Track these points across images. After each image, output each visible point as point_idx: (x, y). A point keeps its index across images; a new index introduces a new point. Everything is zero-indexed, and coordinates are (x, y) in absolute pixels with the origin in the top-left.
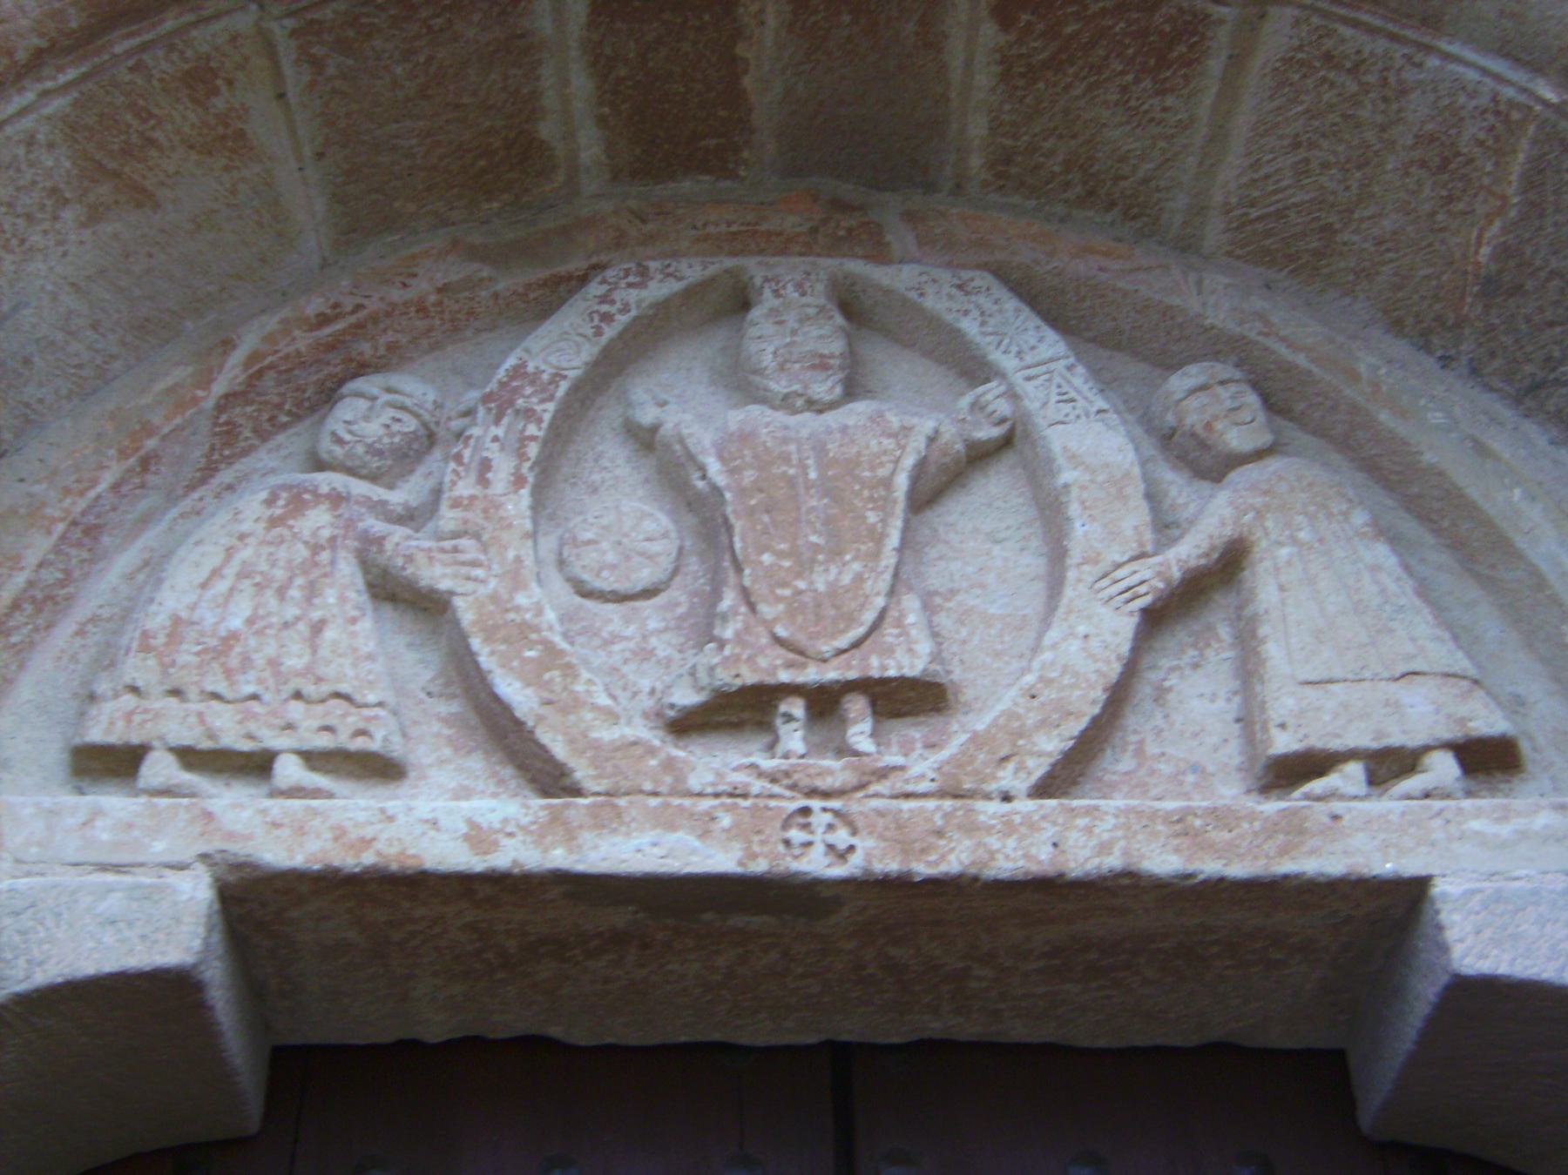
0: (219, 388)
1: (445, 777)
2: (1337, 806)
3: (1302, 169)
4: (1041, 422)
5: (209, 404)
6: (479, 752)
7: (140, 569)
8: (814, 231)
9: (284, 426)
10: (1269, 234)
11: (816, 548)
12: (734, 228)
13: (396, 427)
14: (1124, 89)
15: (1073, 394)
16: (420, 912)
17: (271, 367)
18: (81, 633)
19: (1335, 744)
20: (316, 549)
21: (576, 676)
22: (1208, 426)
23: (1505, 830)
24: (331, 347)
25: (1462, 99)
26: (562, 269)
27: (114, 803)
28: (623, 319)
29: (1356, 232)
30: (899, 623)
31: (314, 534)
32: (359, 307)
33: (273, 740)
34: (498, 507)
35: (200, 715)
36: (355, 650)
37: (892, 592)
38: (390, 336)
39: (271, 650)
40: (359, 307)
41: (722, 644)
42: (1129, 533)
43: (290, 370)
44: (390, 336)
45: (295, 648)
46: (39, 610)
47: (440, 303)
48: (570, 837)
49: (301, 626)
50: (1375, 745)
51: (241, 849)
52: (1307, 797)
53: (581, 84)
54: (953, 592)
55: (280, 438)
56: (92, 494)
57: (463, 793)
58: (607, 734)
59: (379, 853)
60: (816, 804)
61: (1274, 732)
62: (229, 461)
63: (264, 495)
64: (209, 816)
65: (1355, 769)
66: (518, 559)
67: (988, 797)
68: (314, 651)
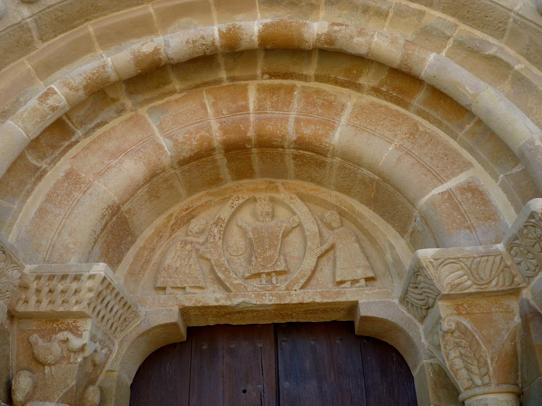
0: (171, 223)
1: (211, 289)
2: (346, 290)
3: (344, 181)
4: (303, 224)
5: (170, 226)
6: (242, 48)
7: (161, 254)
8: (267, 188)
9: (182, 227)
10: (341, 188)
11: (267, 249)
12: (253, 188)
13: (200, 228)
14: (315, 169)
15: (309, 218)
16: (209, 310)
17: (179, 218)
18: (153, 266)
19: (346, 279)
20: (189, 252)
21: (230, 273)
22: (330, 223)
23: (370, 292)
24: (189, 214)
25: (365, 176)
26: (225, 197)
27: (162, 297)
28: (235, 207)
29: (354, 190)
30: (280, 261)
31: (189, 249)
32: (193, 206)
33: (185, 285)
34: (217, 243)
35: (174, 281)
36: (196, 269)
37: (279, 255)
38: (198, 210)
39: (183, 270)
40: (193, 206)
41: (253, 266)
42: (316, 243)
43: (182, 218)
44: (198, 210)
45: (187, 269)
46: (147, 263)
47: (206, 204)
48: (231, 300)
49: (188, 266)
50: (353, 279)
51: (182, 303)
52: (342, 288)
53: (226, 170)
54: (290, 253)
55: (181, 229)
56: (153, 243)
57: (214, 292)
58: (235, 282)
59: (202, 303)
60: (267, 292)
61: (337, 277)
62: (173, 234)
63: (180, 243)
64: (177, 298)
65: (349, 283)
66: (220, 252)
67: (293, 290)
68: (190, 269)
